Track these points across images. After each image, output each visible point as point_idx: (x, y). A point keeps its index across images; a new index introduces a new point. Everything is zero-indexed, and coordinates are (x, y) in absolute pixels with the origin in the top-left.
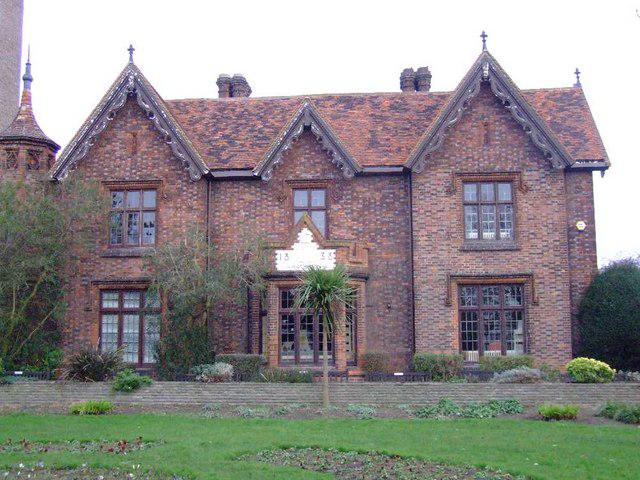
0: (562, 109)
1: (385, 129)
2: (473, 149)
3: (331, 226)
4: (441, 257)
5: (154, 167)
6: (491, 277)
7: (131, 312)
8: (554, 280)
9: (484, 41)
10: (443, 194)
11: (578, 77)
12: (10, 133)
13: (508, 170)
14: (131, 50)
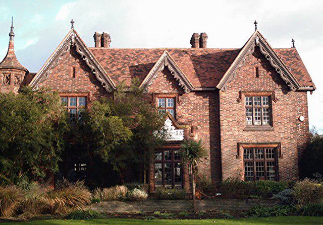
0: (288, 60)
1: (201, 68)
2: (250, 80)
3: (177, 117)
4: (235, 134)
5: (85, 85)
6: (259, 144)
7: (159, 162)
8: (290, 146)
9: (256, 26)
10: (236, 102)
11: (293, 43)
12: (3, 65)
13: (268, 90)
14: (72, 22)
